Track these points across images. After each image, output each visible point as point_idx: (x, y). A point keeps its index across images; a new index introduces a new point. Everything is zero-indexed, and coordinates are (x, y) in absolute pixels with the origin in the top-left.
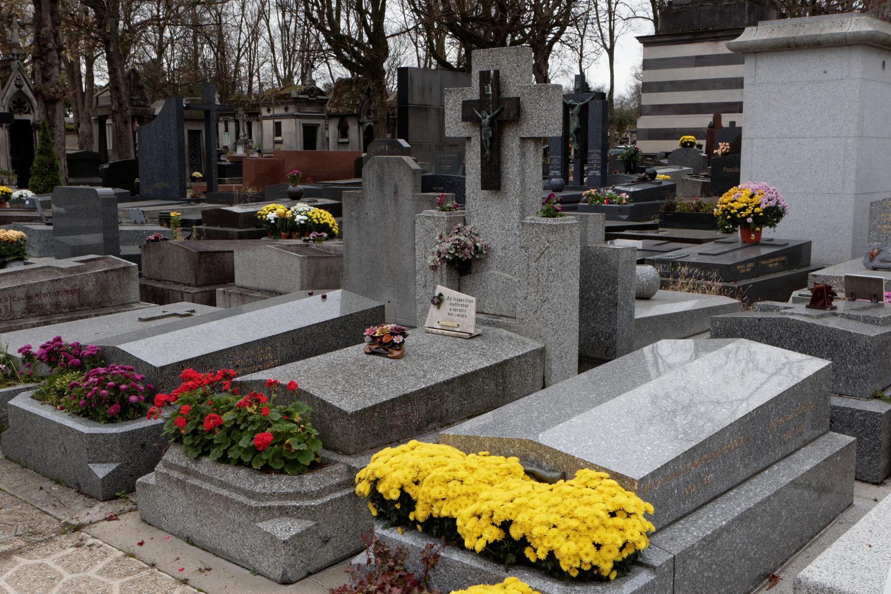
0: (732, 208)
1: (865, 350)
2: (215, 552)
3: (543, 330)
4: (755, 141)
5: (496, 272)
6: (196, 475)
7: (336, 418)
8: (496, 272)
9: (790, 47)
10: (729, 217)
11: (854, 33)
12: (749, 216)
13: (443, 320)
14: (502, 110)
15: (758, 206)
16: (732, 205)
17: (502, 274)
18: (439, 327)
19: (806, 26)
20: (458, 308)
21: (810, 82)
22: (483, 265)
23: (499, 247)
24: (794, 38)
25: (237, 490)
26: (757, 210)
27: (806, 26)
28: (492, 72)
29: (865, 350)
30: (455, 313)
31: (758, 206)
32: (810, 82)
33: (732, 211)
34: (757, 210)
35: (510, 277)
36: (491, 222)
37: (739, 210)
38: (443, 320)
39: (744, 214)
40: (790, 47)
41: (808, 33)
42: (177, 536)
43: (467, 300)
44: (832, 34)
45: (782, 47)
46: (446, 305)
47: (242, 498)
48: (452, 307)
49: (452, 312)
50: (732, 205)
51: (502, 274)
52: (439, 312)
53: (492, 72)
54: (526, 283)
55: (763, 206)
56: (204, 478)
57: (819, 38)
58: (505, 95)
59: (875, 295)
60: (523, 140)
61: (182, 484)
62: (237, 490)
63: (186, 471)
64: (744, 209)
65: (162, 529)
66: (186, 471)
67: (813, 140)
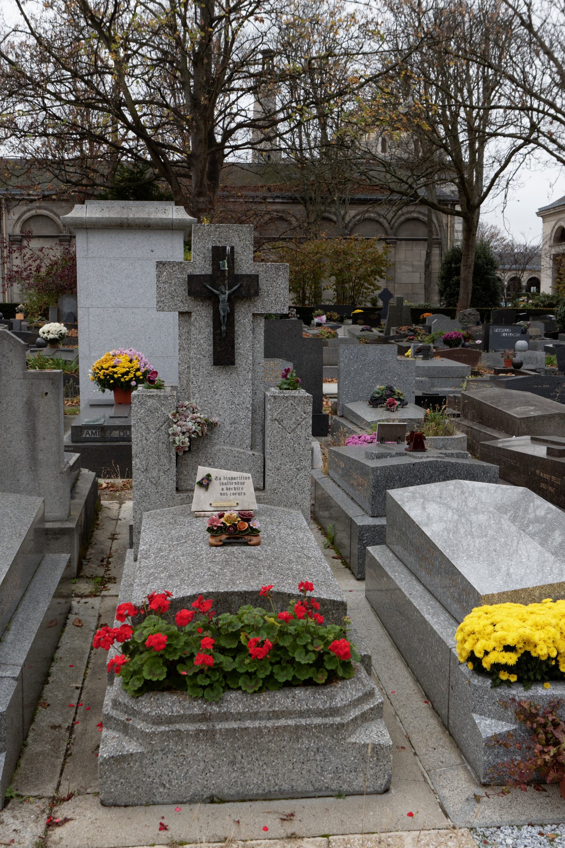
0: (116, 373)
1: (494, 477)
2: (293, 795)
3: (299, 497)
4: (91, 310)
5: (225, 448)
6: (226, 717)
7: (327, 612)
8: (225, 448)
9: (122, 226)
10: (112, 381)
11: (180, 220)
12: (131, 380)
13: (215, 501)
14: (241, 286)
15: (138, 370)
16: (115, 370)
17: (233, 449)
18: (212, 509)
19: (133, 209)
20: (232, 486)
21: (139, 259)
22: (206, 442)
23: (228, 421)
24: (127, 218)
25: (302, 714)
26: (138, 373)
27: (133, 209)
28: (228, 248)
29: (494, 477)
30: (229, 492)
31: (138, 370)
32: (139, 259)
33: (116, 376)
34: (138, 373)
35: (242, 450)
36: (217, 397)
37: (123, 374)
38: (215, 501)
39: (127, 378)
40: (122, 226)
41: (137, 216)
42: (192, 801)
43: (241, 478)
44: (161, 219)
45: (115, 226)
46: (215, 486)
47: (318, 721)
48: (224, 487)
49: (225, 491)
50: (115, 370)
51: (233, 449)
52: (207, 494)
53: (228, 248)
54: (280, 454)
55: (143, 370)
56: (240, 717)
57: (150, 221)
58: (236, 272)
59: (399, 438)
60: (254, 315)
61: (210, 735)
62: (302, 714)
63: (204, 718)
64: (127, 373)
65: (158, 804)
66: (204, 718)
67: (146, 310)
